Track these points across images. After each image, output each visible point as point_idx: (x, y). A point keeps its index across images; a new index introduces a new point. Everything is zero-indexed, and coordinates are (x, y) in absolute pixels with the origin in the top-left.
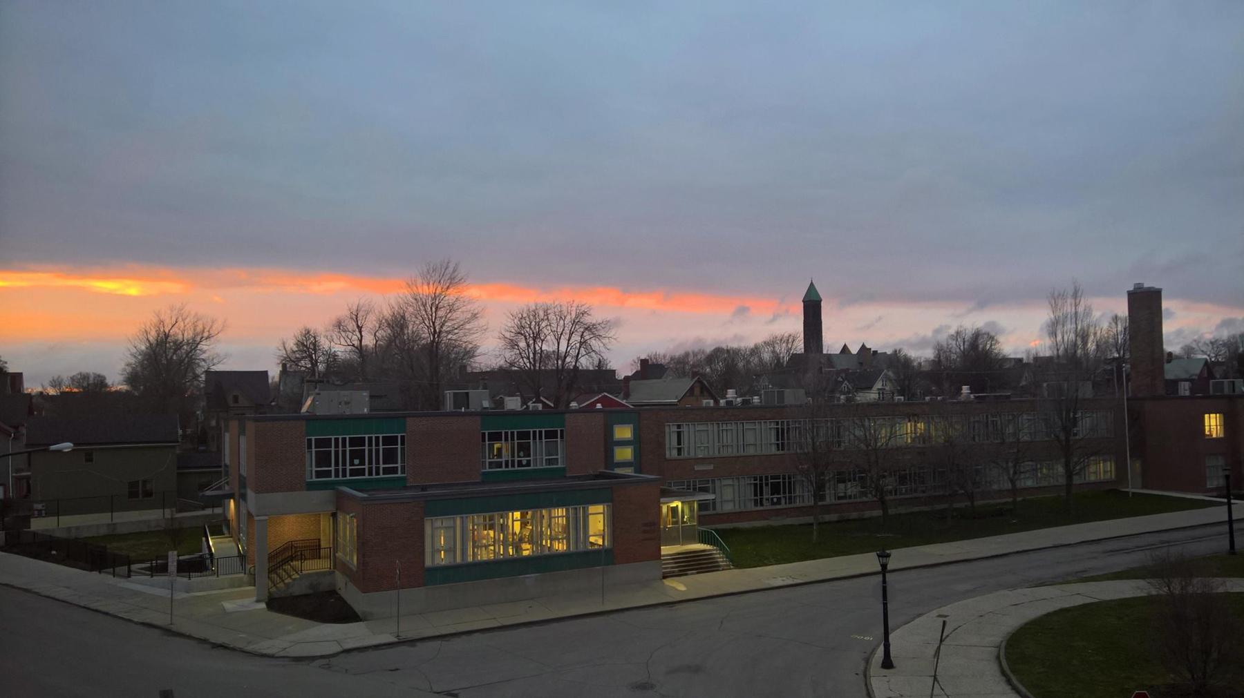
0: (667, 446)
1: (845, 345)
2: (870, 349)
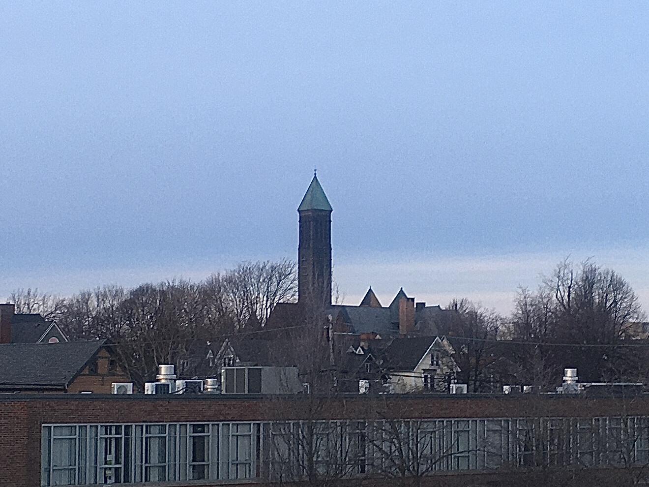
0: (44, 465)
1: (370, 290)
2: (413, 300)
